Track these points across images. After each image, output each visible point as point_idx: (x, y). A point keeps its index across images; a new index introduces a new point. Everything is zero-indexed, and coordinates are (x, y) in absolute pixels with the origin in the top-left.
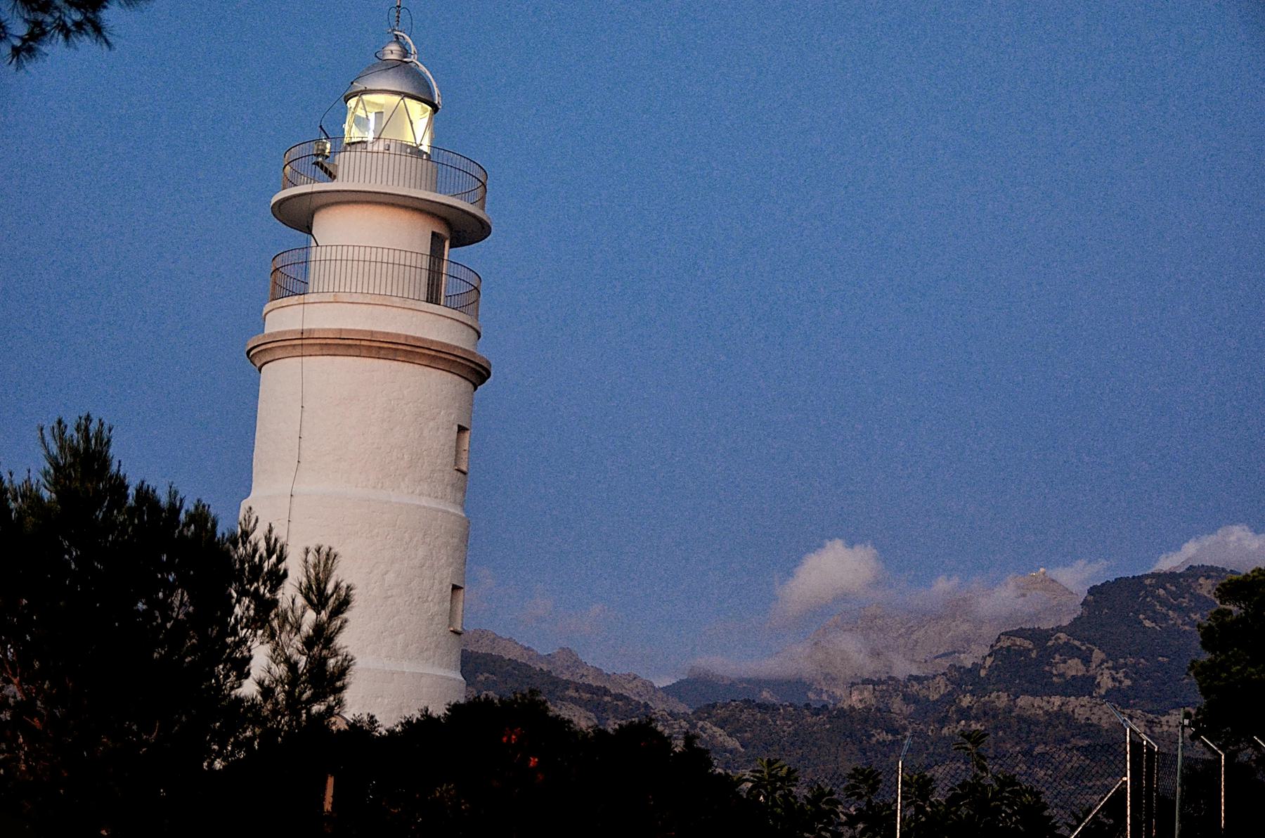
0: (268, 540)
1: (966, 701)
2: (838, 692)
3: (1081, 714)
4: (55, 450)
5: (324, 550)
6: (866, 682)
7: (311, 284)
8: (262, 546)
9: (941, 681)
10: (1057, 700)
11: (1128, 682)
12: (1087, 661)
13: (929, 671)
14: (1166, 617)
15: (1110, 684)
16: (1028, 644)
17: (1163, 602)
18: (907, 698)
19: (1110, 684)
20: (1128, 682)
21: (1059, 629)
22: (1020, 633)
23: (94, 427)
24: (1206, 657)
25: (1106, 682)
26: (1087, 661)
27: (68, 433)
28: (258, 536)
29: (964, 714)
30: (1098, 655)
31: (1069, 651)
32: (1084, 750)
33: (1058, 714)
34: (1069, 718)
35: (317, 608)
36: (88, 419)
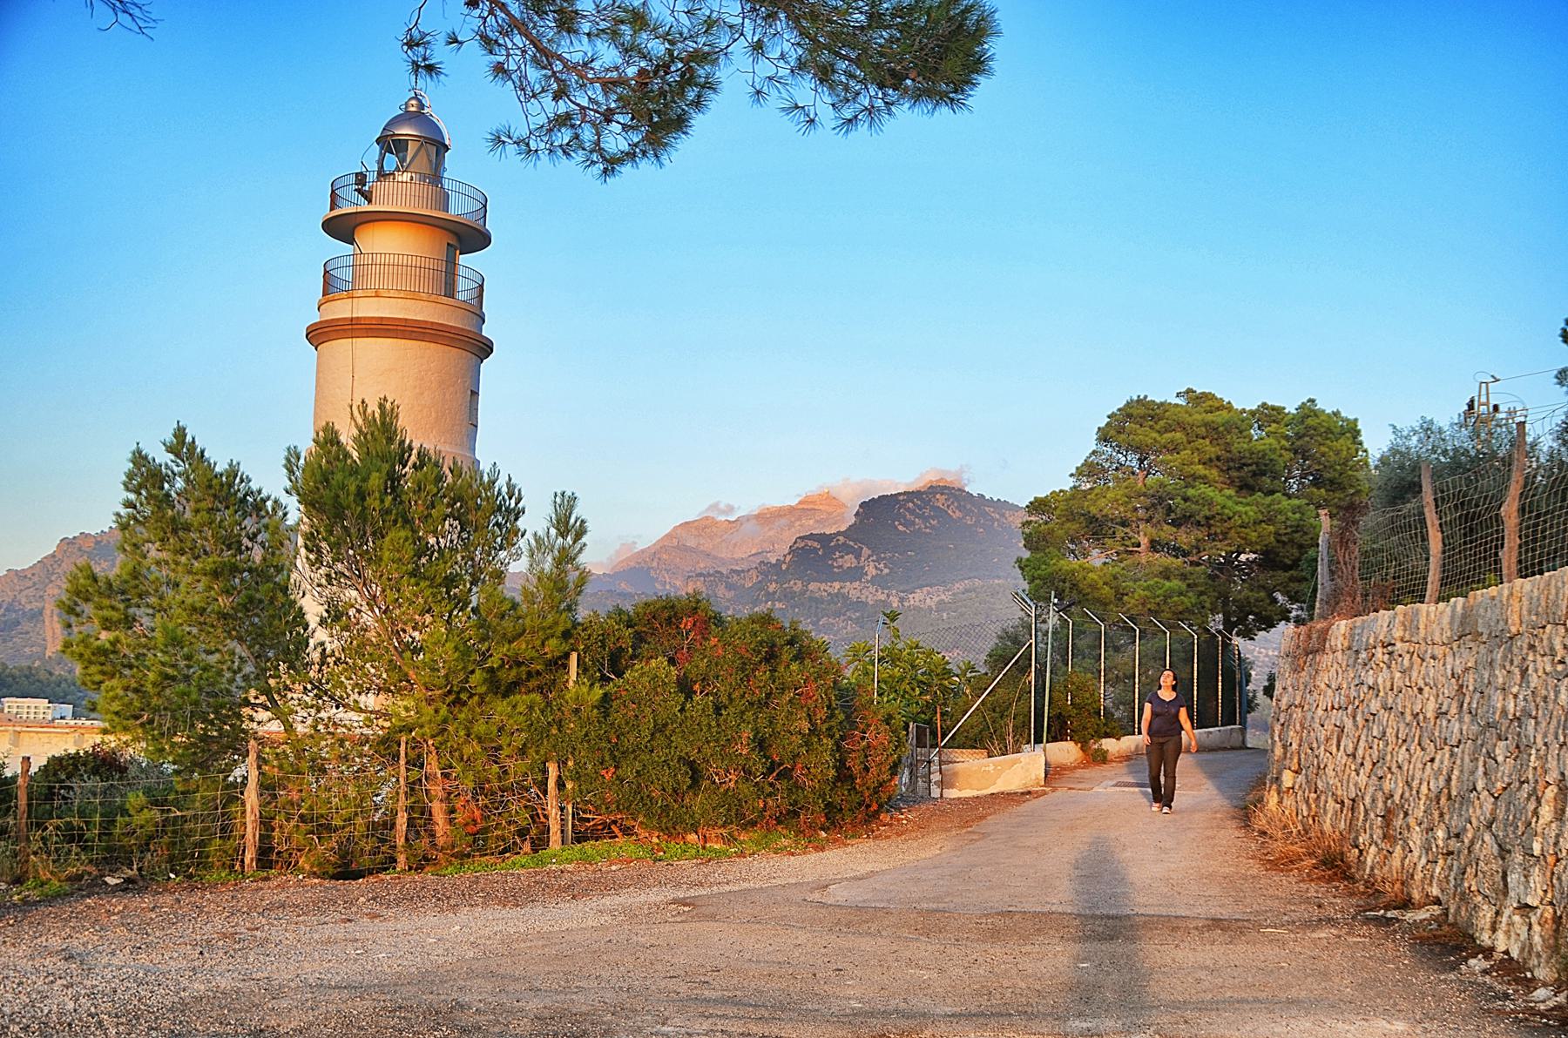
0: (508, 484)
1: (772, 587)
2: (678, 583)
3: (854, 595)
4: (360, 421)
5: (568, 493)
6: (701, 575)
7: (1514, 560)
8: (505, 489)
9: (754, 573)
10: (837, 585)
11: (886, 571)
12: (858, 557)
13: (745, 567)
14: (913, 523)
15: (874, 572)
16: (816, 544)
17: (912, 512)
18: (729, 587)
19: (874, 572)
20: (886, 571)
21: (839, 533)
22: (811, 537)
23: (388, 405)
24: (1027, 554)
25: (871, 571)
26: (858, 557)
27: (369, 411)
28: (501, 482)
29: (770, 596)
30: (866, 551)
31: (846, 549)
32: (857, 621)
33: (837, 595)
34: (846, 597)
35: (563, 535)
36: (385, 399)
